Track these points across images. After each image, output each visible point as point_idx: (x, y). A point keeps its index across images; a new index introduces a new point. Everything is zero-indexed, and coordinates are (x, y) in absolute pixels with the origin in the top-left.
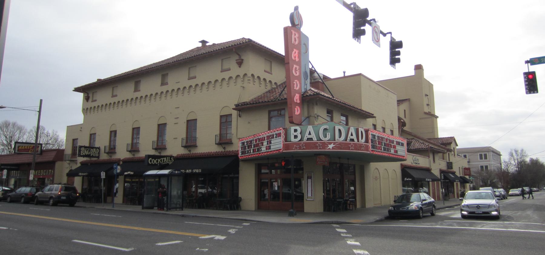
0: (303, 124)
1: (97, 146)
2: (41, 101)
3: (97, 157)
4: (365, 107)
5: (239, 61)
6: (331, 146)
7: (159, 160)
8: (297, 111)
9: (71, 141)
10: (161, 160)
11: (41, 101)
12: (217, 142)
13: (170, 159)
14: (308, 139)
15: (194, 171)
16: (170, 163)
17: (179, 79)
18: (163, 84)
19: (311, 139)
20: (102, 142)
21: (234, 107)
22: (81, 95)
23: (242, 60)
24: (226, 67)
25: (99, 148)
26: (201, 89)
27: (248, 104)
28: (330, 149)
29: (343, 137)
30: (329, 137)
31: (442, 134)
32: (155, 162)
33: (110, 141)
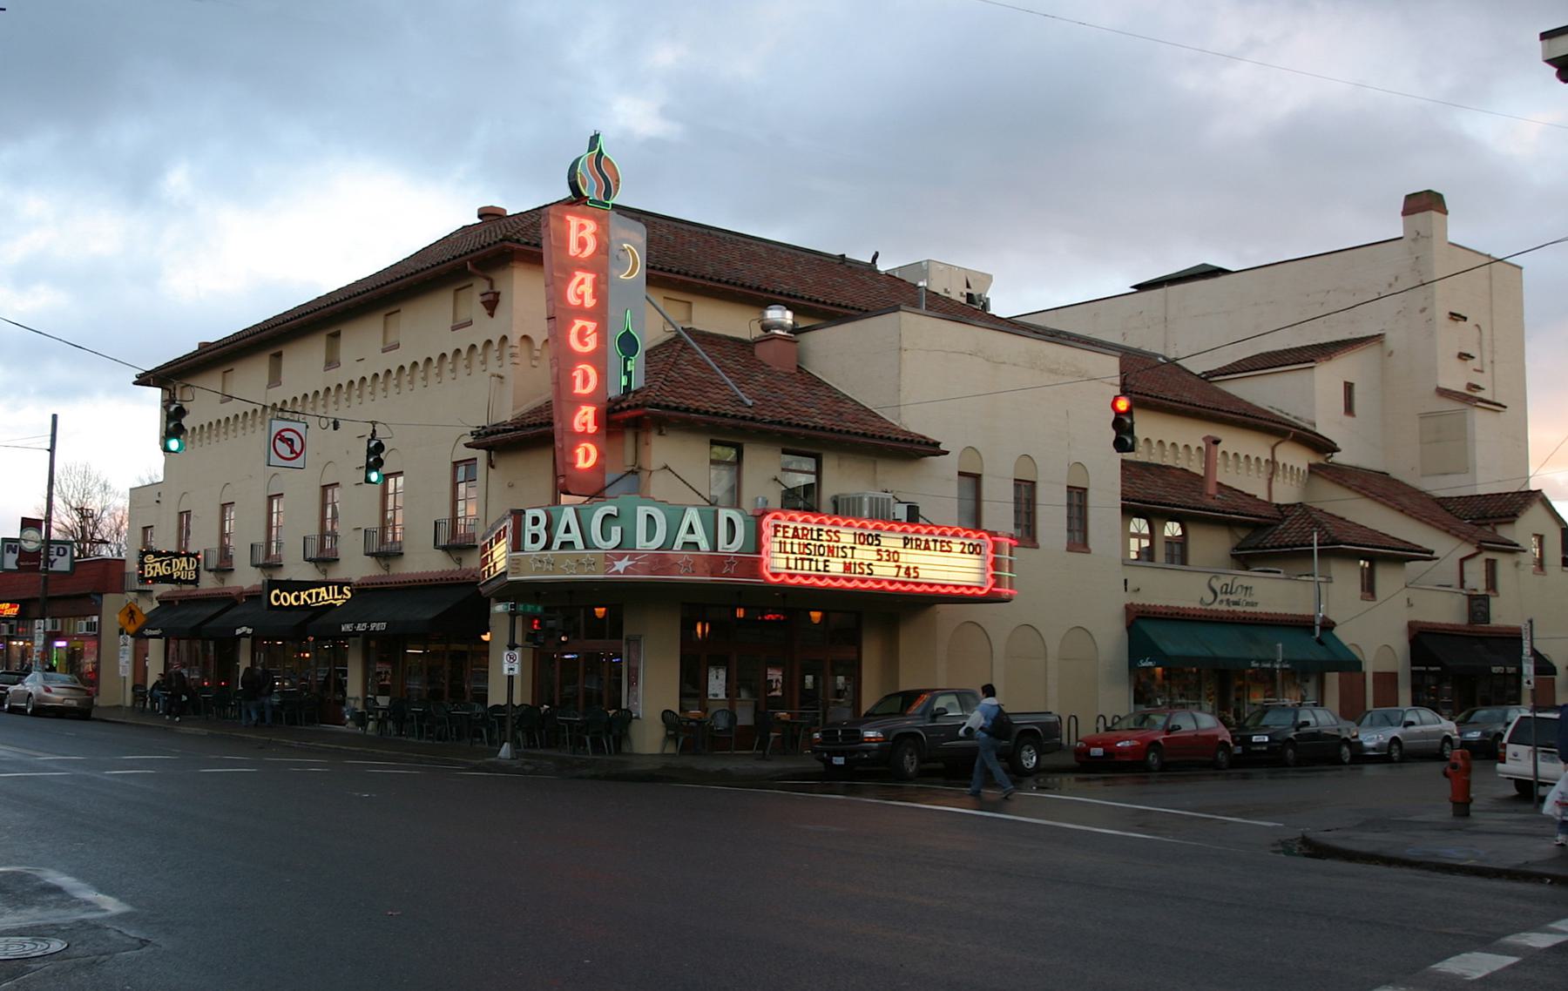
0: (608, 492)
1: (192, 550)
2: (55, 417)
3: (191, 582)
4: (914, 421)
5: (491, 297)
6: (621, 565)
7: (303, 595)
8: (585, 457)
9: (139, 533)
10: (310, 596)
11: (55, 417)
12: (443, 541)
13: (340, 592)
14: (564, 545)
15: (373, 626)
16: (339, 603)
17: (362, 345)
18: (331, 363)
19: (571, 544)
20: (203, 540)
21: (470, 440)
22: (156, 393)
23: (498, 294)
24: (463, 316)
25: (195, 555)
26: (397, 386)
27: (499, 432)
28: (618, 572)
29: (659, 539)
30: (616, 538)
31: (1533, 488)
32: (291, 599)
33: (180, 541)
